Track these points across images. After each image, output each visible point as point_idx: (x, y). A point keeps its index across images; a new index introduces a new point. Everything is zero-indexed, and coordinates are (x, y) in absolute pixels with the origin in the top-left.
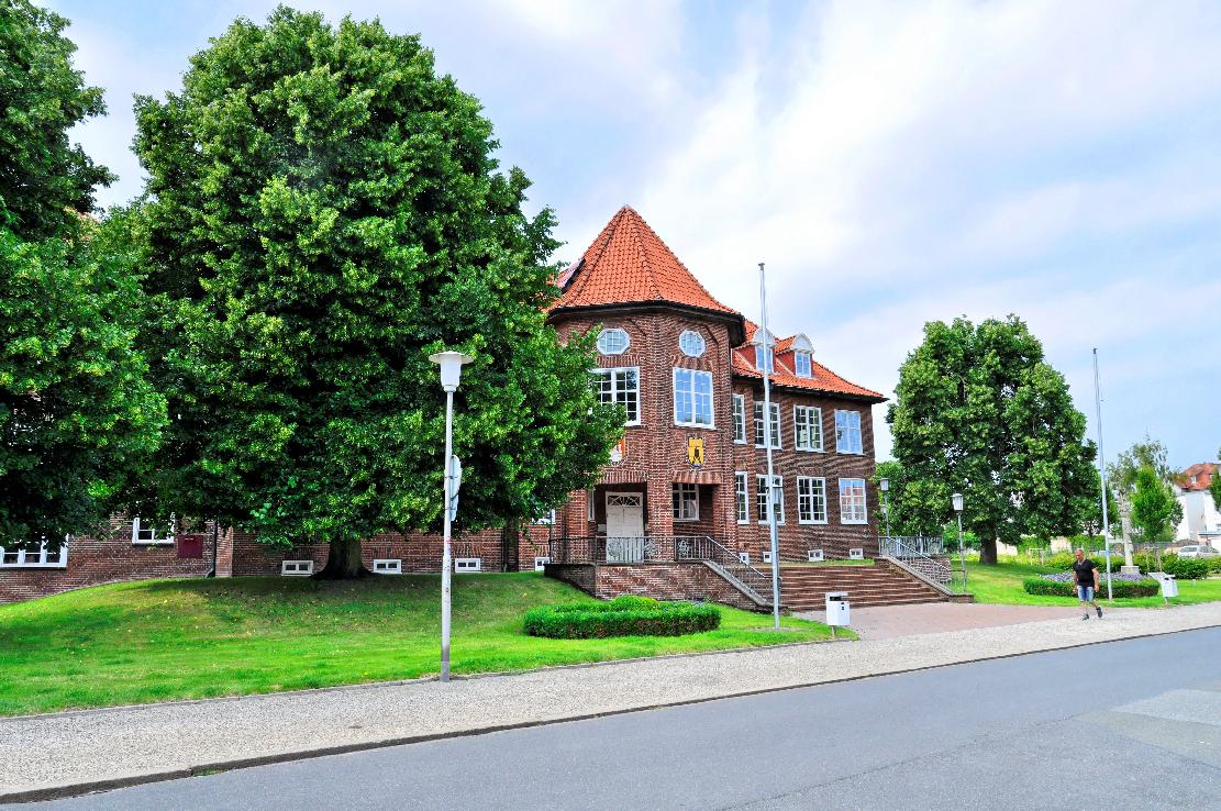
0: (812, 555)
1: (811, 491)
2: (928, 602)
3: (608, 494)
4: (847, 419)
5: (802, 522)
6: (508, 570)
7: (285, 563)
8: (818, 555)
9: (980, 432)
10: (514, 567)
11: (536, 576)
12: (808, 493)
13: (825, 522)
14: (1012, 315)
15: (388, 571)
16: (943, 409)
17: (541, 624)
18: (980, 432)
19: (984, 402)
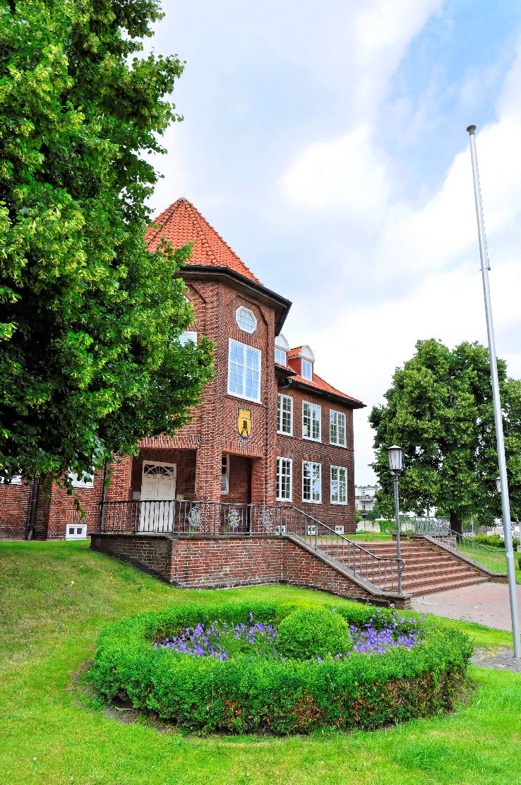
0: (337, 529)
1: (280, 479)
2: (468, 584)
3: (145, 463)
4: (335, 414)
5: (304, 500)
6: (34, 538)
8: (80, 531)
9: (467, 428)
10: (42, 535)
11: (79, 548)
12: (283, 478)
13: (290, 500)
14: (477, 342)
16: (439, 409)
17: (150, 686)
18: (467, 428)
19: (469, 406)
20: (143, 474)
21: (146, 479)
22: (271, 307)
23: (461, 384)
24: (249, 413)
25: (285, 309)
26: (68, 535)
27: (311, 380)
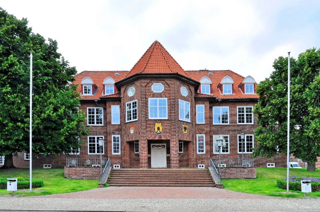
7: (267, 164)
8: (118, 167)
15: (271, 166)
20: (151, 148)
21: (152, 150)
22: (193, 85)
23: (13, 82)
24: (161, 124)
25: (198, 85)
26: (199, 168)
27: (231, 93)
